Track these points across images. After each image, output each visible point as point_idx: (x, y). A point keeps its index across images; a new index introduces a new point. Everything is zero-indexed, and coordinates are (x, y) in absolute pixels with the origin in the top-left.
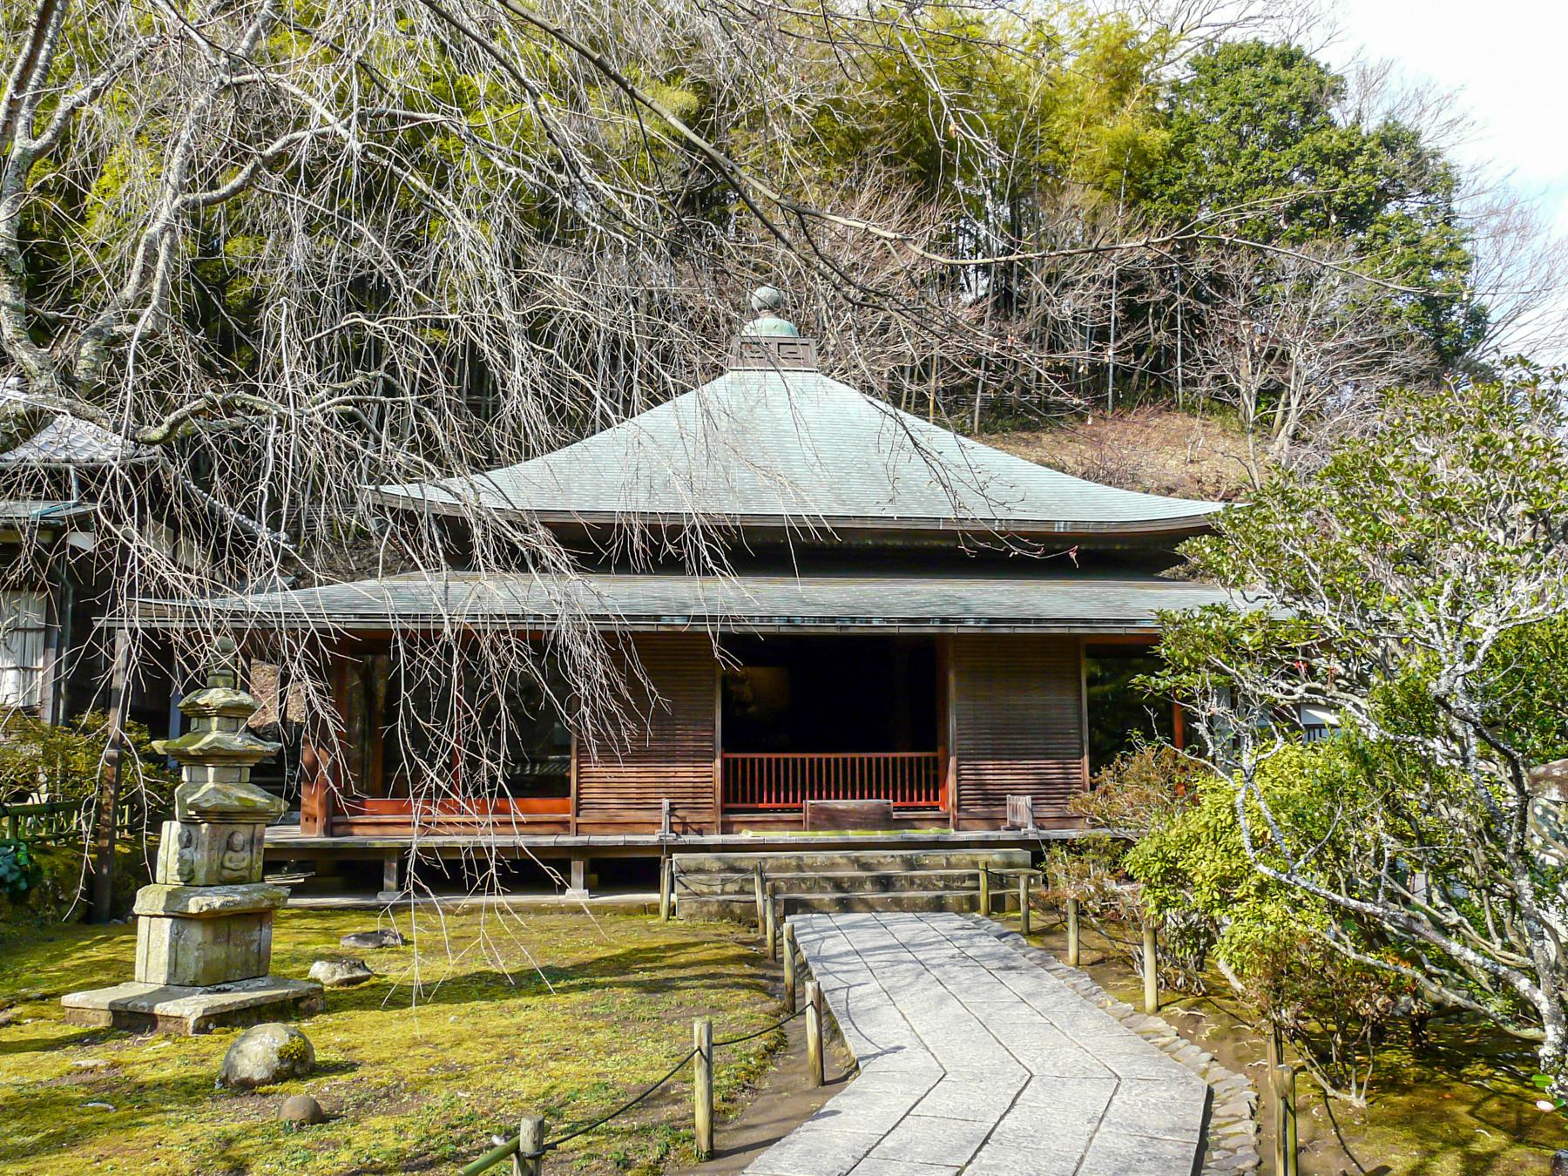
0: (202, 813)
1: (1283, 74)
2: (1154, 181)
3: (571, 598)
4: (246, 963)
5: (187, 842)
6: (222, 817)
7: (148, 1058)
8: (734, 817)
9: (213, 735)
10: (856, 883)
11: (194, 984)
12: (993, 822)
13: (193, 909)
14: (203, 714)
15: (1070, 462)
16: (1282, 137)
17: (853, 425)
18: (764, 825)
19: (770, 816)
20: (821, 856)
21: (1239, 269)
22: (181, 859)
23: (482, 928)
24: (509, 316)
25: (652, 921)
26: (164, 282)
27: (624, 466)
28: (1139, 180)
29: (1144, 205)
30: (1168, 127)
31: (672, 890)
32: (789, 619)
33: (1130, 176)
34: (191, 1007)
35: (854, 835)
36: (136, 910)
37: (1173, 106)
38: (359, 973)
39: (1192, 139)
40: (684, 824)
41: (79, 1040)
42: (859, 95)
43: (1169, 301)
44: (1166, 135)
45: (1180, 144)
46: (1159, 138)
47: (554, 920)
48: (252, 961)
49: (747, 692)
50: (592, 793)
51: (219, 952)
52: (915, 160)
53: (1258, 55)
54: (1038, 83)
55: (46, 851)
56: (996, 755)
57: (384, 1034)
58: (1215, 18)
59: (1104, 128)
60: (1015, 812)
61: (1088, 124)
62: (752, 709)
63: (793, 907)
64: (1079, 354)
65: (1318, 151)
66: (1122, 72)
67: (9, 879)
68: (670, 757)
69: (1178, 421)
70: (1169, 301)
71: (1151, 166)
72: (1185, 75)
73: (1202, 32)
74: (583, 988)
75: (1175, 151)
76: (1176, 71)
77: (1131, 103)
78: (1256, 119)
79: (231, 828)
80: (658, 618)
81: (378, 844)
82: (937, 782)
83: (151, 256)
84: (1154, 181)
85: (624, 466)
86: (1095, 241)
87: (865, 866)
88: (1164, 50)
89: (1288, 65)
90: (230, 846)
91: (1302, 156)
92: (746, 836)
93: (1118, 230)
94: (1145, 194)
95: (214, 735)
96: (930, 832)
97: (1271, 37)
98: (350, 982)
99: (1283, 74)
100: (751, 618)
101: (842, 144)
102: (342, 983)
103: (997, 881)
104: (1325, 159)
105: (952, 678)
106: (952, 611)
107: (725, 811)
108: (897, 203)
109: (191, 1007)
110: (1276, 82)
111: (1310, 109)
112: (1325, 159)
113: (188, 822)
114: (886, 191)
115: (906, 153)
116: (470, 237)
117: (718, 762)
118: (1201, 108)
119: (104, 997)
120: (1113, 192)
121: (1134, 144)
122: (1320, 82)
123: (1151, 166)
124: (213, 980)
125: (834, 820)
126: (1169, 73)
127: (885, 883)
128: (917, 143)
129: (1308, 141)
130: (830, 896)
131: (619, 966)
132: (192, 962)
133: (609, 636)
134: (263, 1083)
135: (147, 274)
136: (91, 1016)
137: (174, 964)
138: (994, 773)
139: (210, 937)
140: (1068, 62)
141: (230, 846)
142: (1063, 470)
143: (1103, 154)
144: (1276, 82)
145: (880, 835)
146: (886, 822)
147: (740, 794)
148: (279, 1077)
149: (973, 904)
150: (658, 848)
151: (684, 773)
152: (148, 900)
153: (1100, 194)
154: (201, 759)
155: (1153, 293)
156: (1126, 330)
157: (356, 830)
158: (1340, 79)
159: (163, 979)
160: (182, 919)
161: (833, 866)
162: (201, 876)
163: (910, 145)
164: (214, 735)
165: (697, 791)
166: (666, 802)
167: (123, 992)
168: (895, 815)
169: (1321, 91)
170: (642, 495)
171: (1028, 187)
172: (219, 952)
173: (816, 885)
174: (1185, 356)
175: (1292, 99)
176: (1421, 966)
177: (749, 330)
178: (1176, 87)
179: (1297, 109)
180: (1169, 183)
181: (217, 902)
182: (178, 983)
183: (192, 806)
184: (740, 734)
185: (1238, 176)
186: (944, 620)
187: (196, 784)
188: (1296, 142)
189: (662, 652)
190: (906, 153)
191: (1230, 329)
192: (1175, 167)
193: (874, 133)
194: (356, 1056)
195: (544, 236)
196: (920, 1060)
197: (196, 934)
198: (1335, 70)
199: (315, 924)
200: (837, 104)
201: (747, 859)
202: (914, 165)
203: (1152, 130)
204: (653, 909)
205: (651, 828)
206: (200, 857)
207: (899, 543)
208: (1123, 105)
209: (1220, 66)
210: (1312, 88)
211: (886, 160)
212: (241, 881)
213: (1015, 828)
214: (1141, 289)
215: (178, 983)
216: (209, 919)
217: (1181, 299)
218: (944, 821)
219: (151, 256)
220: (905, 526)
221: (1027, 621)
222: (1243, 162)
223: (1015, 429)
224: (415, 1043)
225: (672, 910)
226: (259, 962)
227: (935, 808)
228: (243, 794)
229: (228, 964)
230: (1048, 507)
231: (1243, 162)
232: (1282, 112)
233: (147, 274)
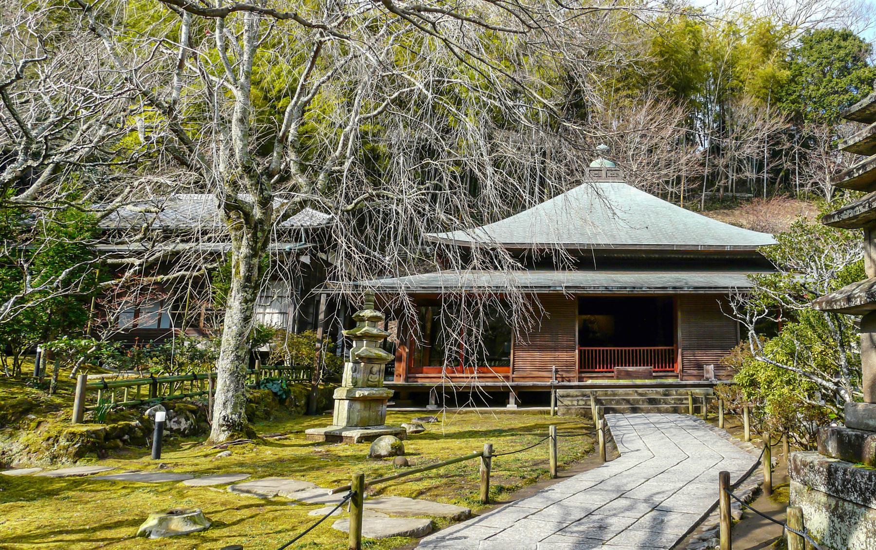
0: (361, 358)
1: (843, 44)
2: (783, 94)
3: (515, 280)
4: (376, 419)
5: (354, 370)
6: (369, 360)
7: (338, 449)
8: (583, 375)
9: (366, 328)
10: (638, 401)
11: (356, 426)
12: (701, 377)
13: (357, 396)
14: (362, 320)
15: (745, 223)
16: (844, 71)
17: (639, 205)
18: (597, 378)
19: (600, 375)
20: (621, 390)
21: (822, 133)
22: (353, 378)
23: (474, 417)
24: (486, 158)
25: (546, 416)
26: (351, 149)
27: (540, 223)
28: (776, 92)
29: (779, 104)
30: (790, 69)
31: (556, 405)
32: (606, 288)
33: (772, 92)
34: (356, 433)
35: (639, 382)
36: (334, 397)
37: (793, 59)
38: (420, 429)
39: (801, 74)
40: (562, 378)
41: (313, 445)
42: (645, 58)
43: (792, 148)
44: (789, 73)
45: (794, 76)
46: (786, 74)
47: (502, 416)
48: (379, 418)
49: (595, 326)
50: (519, 364)
51: (366, 414)
52: (672, 86)
53: (831, 35)
54: (729, 50)
55: (292, 385)
56: (699, 347)
57: (433, 446)
58: (813, 18)
59: (760, 70)
60: (708, 372)
61: (753, 68)
62: (598, 334)
63: (607, 411)
64: (750, 174)
65: (859, 78)
66: (768, 43)
67: (279, 393)
68: (555, 349)
69: (797, 204)
70: (792, 148)
71: (782, 87)
72: (799, 45)
73: (806, 25)
74: (512, 435)
75: (792, 80)
76: (795, 44)
77: (772, 58)
78: (831, 64)
79: (371, 365)
80: (550, 287)
81: (428, 385)
82: (673, 361)
83: (347, 139)
84: (783, 94)
85: (540, 223)
86: (758, 123)
87: (640, 395)
88: (790, 32)
89: (845, 40)
90: (371, 372)
91: (851, 81)
92: (589, 382)
93: (767, 117)
94: (779, 100)
95: (366, 328)
96: (670, 381)
97: (838, 27)
98: (416, 432)
99: (843, 44)
100: (590, 287)
101: (630, 81)
102: (413, 432)
103: (695, 400)
104: (862, 82)
105: (679, 314)
106: (678, 284)
107: (580, 372)
108: (662, 106)
109: (356, 433)
110: (839, 47)
111: (856, 59)
112: (862, 82)
113: (356, 362)
114: (657, 101)
115: (668, 83)
116: (471, 126)
117: (577, 351)
118: (805, 60)
119: (323, 430)
120: (765, 99)
121: (774, 77)
122: (860, 47)
123: (782, 87)
124: (363, 424)
125: (629, 375)
126: (791, 45)
127: (652, 401)
128: (672, 79)
129: (855, 73)
130: (624, 406)
131: (528, 429)
132: (356, 417)
133: (528, 296)
134: (385, 456)
135: (345, 145)
136: (316, 437)
137: (349, 418)
138: (701, 356)
139: (363, 407)
140: (744, 42)
141: (371, 372)
142: (741, 226)
143: (759, 82)
144: (839, 47)
145: (647, 382)
146: (649, 376)
147: (587, 365)
148: (391, 455)
149: (687, 410)
150: (550, 387)
151: (564, 356)
152: (339, 393)
153: (758, 100)
154: (359, 338)
155: (784, 145)
156: (771, 162)
157: (419, 380)
158: (870, 45)
159: (344, 424)
160: (352, 399)
161: (627, 394)
162: (360, 383)
163: (680, 75)
164: (366, 328)
165: (568, 367)
166: (554, 368)
167: (328, 429)
168: (654, 374)
169: (860, 51)
170: (545, 236)
171: (727, 95)
172: (366, 414)
173: (618, 402)
174: (800, 174)
175: (847, 55)
176: (835, 406)
177: (595, 164)
178: (794, 51)
179: (850, 59)
180: (791, 95)
181: (366, 393)
182: (350, 425)
183: (357, 356)
184: (586, 338)
185: (822, 90)
186: (674, 288)
187: (358, 348)
188: (849, 74)
189: (551, 300)
190: (668, 83)
191: (818, 161)
192: (793, 86)
193: (653, 75)
194: (420, 451)
195: (502, 126)
196: (646, 453)
197: (358, 406)
198: (867, 41)
199: (401, 416)
200: (636, 63)
201: (588, 391)
202: (671, 89)
203: (782, 71)
204: (548, 413)
205: (547, 379)
206: (360, 376)
207: (657, 256)
208: (769, 59)
209: (814, 40)
210: (856, 49)
211: (659, 87)
212: (375, 386)
213: (707, 379)
214: (778, 143)
215: (350, 425)
216: (363, 400)
217: (797, 147)
218: (677, 377)
219: (347, 139)
220: (658, 248)
221: (711, 288)
222: (824, 84)
223: (721, 208)
224: (443, 449)
225: (555, 413)
226: (381, 419)
227: (673, 371)
228: (377, 352)
229: (369, 419)
230: (723, 240)
231: (824, 84)
232: (842, 61)
233: (345, 145)
